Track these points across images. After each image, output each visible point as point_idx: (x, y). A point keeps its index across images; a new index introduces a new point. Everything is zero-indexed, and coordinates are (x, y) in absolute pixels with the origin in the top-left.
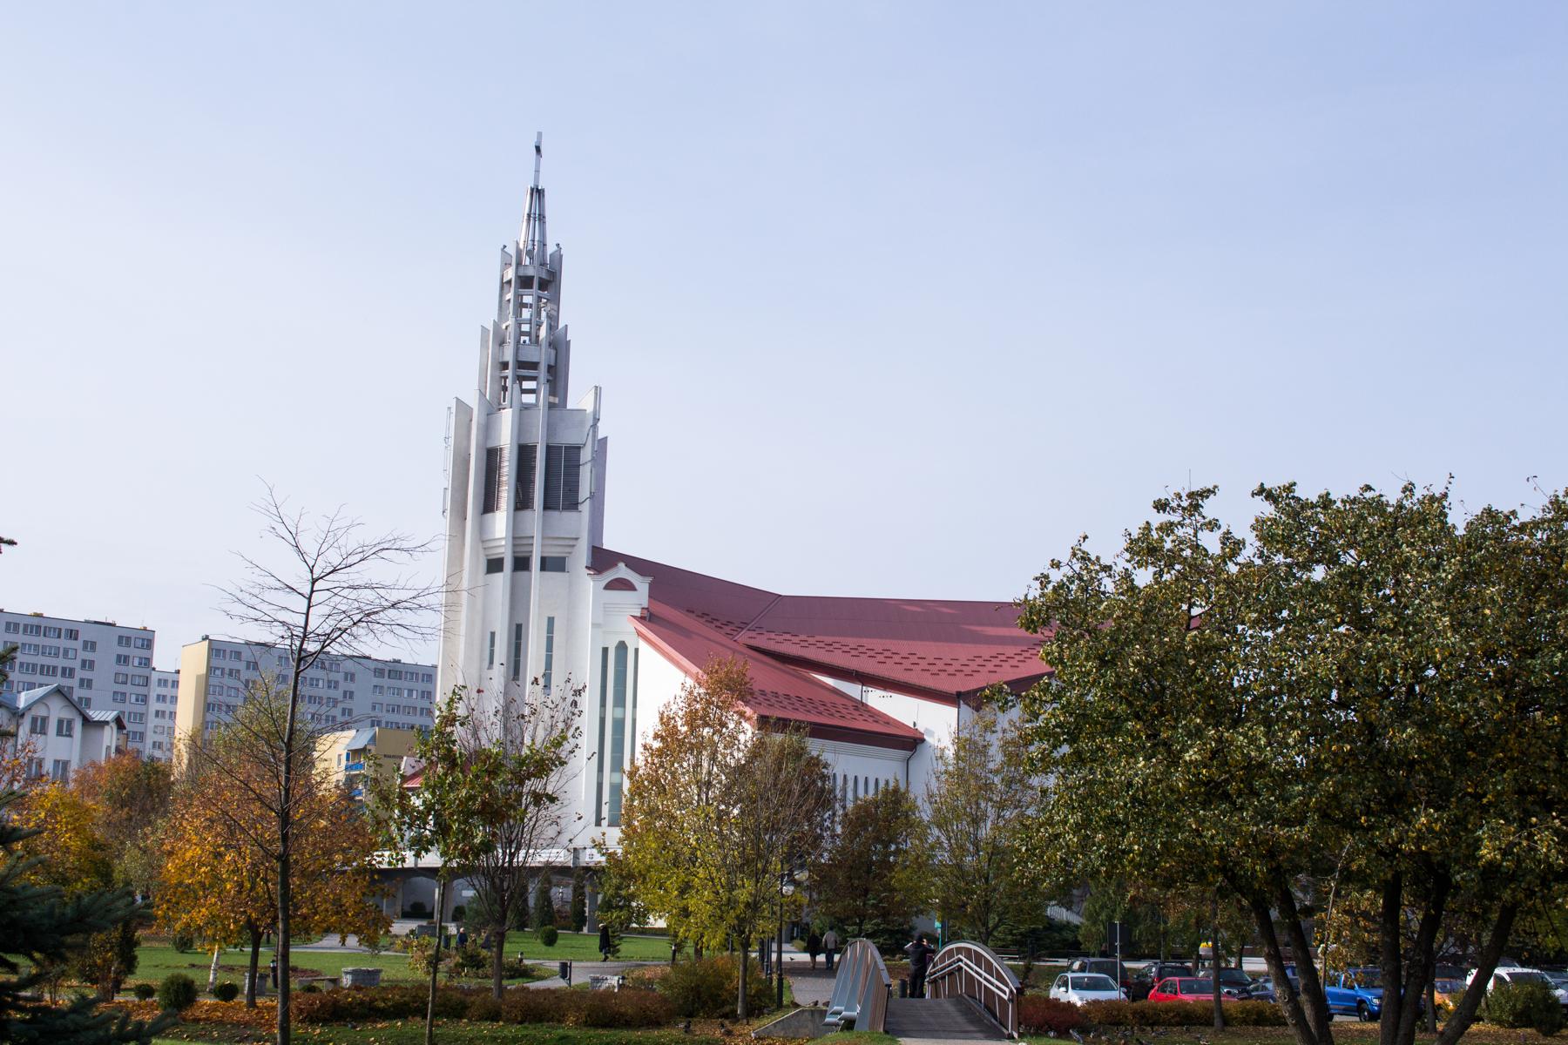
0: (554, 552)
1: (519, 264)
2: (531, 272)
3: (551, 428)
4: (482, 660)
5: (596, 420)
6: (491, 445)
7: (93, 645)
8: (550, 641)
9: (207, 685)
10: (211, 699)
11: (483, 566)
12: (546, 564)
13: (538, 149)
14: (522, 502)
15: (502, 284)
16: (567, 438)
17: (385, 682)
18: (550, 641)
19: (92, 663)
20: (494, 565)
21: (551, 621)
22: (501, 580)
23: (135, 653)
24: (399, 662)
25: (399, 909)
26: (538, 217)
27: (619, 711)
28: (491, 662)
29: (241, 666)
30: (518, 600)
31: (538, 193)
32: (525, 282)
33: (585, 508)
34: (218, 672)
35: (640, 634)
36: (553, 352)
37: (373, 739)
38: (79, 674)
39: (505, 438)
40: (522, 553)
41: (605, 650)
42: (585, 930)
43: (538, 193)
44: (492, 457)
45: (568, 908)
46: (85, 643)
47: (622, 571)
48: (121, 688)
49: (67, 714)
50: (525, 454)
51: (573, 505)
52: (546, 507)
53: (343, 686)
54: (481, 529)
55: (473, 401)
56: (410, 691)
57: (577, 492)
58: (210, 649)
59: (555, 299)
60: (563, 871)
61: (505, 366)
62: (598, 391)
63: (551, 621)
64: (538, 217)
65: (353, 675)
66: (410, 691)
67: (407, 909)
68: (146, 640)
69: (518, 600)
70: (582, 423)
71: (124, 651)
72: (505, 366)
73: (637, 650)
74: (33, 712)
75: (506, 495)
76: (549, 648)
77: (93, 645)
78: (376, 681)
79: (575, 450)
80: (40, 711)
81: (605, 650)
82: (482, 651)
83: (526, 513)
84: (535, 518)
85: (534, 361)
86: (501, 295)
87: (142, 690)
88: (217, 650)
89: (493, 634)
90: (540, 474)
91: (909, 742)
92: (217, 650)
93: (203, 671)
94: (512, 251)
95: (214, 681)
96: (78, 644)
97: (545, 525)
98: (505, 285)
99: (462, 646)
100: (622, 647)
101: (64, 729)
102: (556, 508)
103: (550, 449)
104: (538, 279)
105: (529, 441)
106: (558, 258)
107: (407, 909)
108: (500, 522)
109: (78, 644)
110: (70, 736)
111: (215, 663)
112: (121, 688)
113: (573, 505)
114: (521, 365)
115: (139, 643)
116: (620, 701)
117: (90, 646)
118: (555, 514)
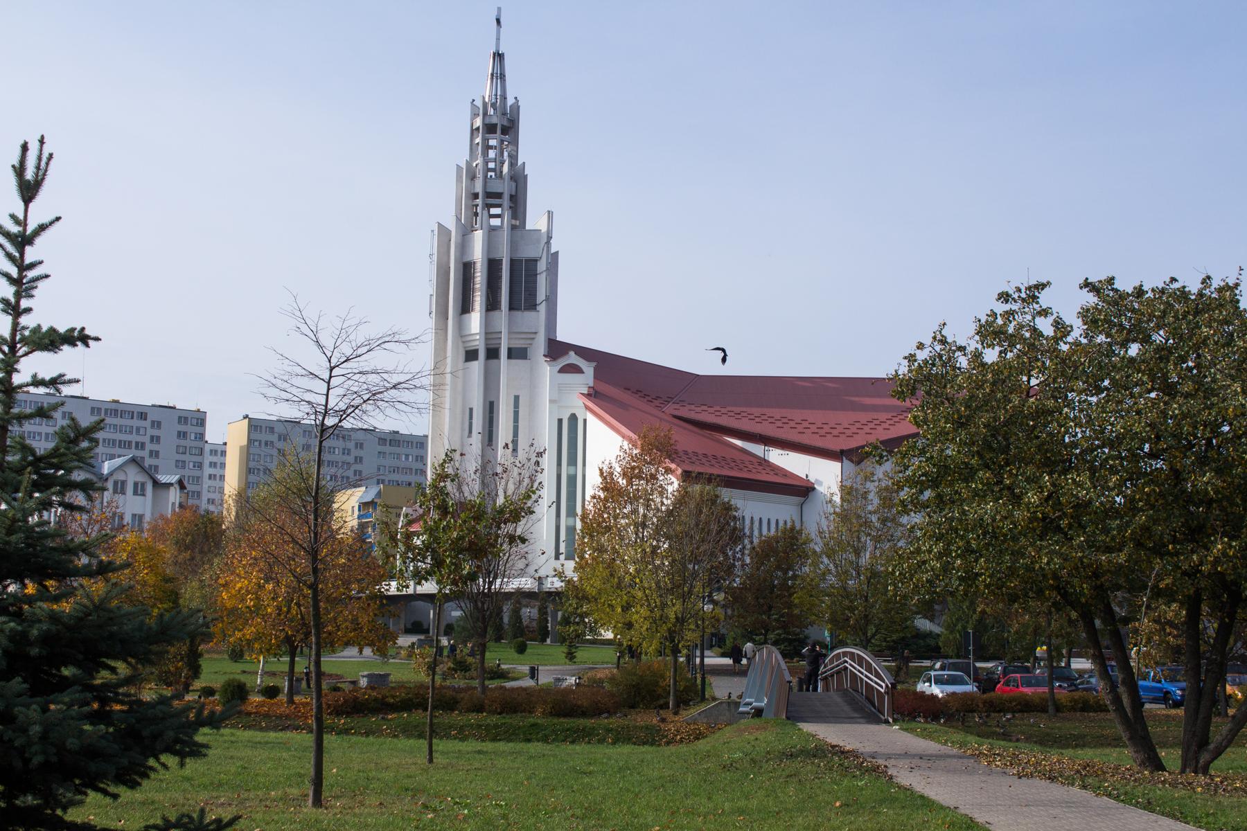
0: (518, 344)
1: (485, 114)
2: (495, 120)
3: (513, 245)
4: (463, 430)
5: (549, 238)
6: (467, 259)
7: (159, 424)
8: (516, 414)
9: (248, 454)
10: (252, 464)
11: (462, 356)
12: (512, 354)
13: (498, 21)
14: (492, 304)
15: (472, 131)
16: (527, 252)
17: (387, 449)
18: (516, 414)
19: (158, 438)
20: (471, 355)
21: (517, 398)
22: (477, 367)
23: (191, 430)
24: (397, 432)
25: (402, 626)
26: (499, 76)
27: (571, 521)
28: (470, 432)
29: (274, 438)
30: (490, 383)
31: (499, 57)
32: (490, 129)
33: (542, 308)
34: (257, 444)
35: (587, 408)
36: (514, 185)
37: (379, 494)
38: (149, 447)
39: (478, 253)
40: (493, 344)
41: (560, 421)
42: (548, 641)
43: (499, 57)
44: (467, 269)
45: (534, 624)
46: (153, 422)
47: (573, 358)
48: (182, 457)
49: (141, 478)
50: (493, 266)
51: (532, 306)
52: (512, 308)
53: (355, 453)
54: (461, 327)
55: (451, 225)
56: (407, 456)
57: (535, 295)
58: (250, 426)
59: (515, 142)
60: (530, 595)
61: (476, 196)
62: (550, 214)
63: (517, 398)
64: (499, 76)
65: (362, 444)
66: (407, 456)
67: (409, 626)
68: (199, 419)
69: (490, 383)
70: (538, 241)
71: (182, 428)
72: (476, 196)
73: (585, 421)
74: (115, 477)
75: (479, 300)
76: (516, 420)
77: (159, 424)
78: (380, 448)
79: (533, 262)
80: (120, 476)
81: (560, 421)
82: (463, 423)
83: (496, 313)
84: (502, 316)
85: (498, 190)
86: (472, 140)
87: (198, 459)
88: (255, 426)
89: (471, 410)
90: (503, 281)
91: (803, 490)
92: (255, 426)
93: (245, 442)
94: (479, 103)
95: (252, 451)
96: (147, 424)
97: (511, 323)
98: (474, 131)
99: (447, 420)
100: (573, 418)
101: (139, 490)
102: (519, 309)
103: (513, 263)
104: (500, 126)
105: (497, 256)
106: (516, 108)
107: (409, 626)
108: (475, 321)
109: (147, 424)
110: (144, 495)
111: (254, 436)
112: (182, 457)
113: (532, 306)
114: (489, 195)
115: (194, 422)
116: (572, 461)
117: (157, 424)
118: (518, 314)
